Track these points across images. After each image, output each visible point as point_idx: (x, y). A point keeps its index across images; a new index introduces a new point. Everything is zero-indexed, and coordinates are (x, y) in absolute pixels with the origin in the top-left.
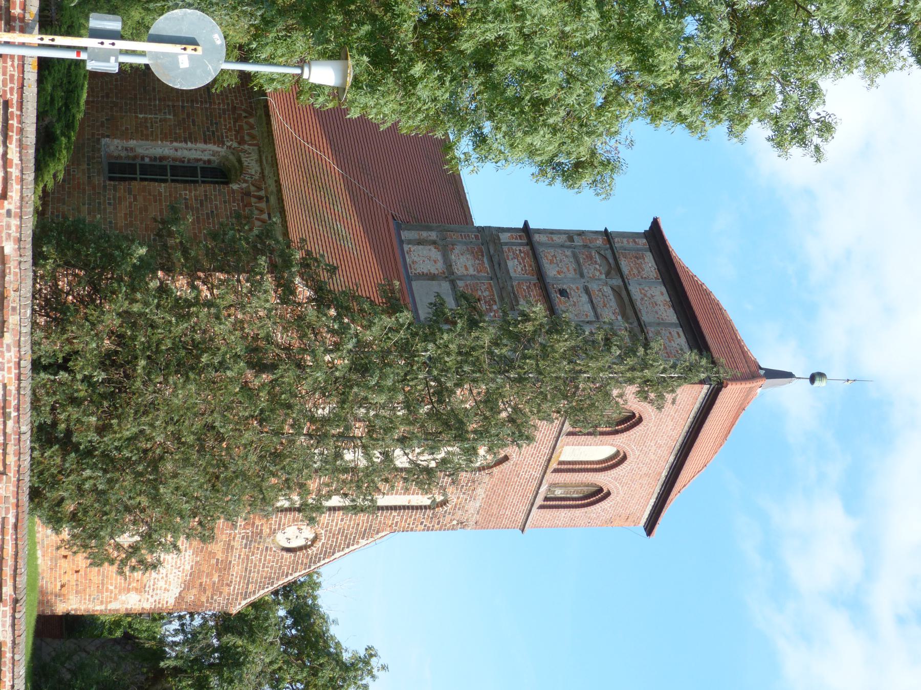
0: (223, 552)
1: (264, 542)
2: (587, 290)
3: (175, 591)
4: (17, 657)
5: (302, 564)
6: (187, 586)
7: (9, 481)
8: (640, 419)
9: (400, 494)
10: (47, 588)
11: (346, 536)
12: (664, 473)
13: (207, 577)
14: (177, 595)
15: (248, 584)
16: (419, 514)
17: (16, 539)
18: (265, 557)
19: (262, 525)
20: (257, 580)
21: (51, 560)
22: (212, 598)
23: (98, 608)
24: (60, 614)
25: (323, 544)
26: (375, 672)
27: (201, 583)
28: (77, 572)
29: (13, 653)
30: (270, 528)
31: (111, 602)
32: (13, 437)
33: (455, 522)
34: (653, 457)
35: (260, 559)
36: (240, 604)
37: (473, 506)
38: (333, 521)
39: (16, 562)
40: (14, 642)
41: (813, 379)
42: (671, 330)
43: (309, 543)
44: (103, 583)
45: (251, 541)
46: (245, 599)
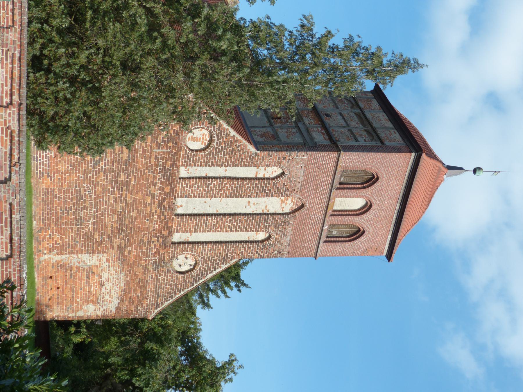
0: (142, 274)
1: (166, 266)
2: (341, 114)
3: (116, 303)
4: (21, 140)
5: (189, 282)
6: (122, 298)
7: (16, 31)
8: (378, 178)
9: (243, 231)
10: (41, 301)
11: (213, 262)
12: (395, 217)
13: (134, 292)
14: (117, 305)
15: (158, 298)
16: (255, 246)
17: (20, 67)
18: (167, 277)
19: (164, 253)
20: (163, 295)
21: (43, 279)
22: (137, 308)
23: (71, 315)
24: (49, 320)
25: (200, 267)
26: (236, 370)
27: (131, 296)
28: (58, 288)
29: (19, 137)
30: (169, 256)
31: (78, 311)
32: (18, 4)
33: (276, 252)
34: (387, 205)
35: (164, 279)
36: (154, 312)
37: (286, 240)
38: (205, 250)
39: (20, 80)
40: (19, 130)
41: (475, 171)
42: (391, 131)
43: (192, 267)
44: (73, 297)
45: (158, 266)
46: (157, 308)
